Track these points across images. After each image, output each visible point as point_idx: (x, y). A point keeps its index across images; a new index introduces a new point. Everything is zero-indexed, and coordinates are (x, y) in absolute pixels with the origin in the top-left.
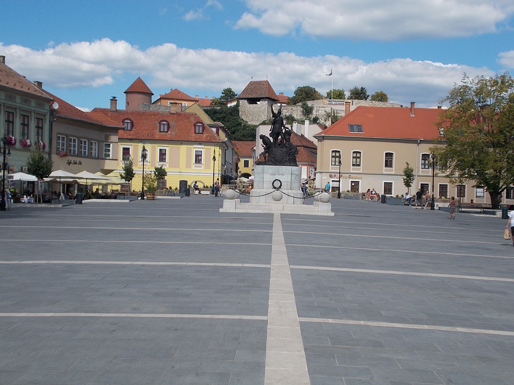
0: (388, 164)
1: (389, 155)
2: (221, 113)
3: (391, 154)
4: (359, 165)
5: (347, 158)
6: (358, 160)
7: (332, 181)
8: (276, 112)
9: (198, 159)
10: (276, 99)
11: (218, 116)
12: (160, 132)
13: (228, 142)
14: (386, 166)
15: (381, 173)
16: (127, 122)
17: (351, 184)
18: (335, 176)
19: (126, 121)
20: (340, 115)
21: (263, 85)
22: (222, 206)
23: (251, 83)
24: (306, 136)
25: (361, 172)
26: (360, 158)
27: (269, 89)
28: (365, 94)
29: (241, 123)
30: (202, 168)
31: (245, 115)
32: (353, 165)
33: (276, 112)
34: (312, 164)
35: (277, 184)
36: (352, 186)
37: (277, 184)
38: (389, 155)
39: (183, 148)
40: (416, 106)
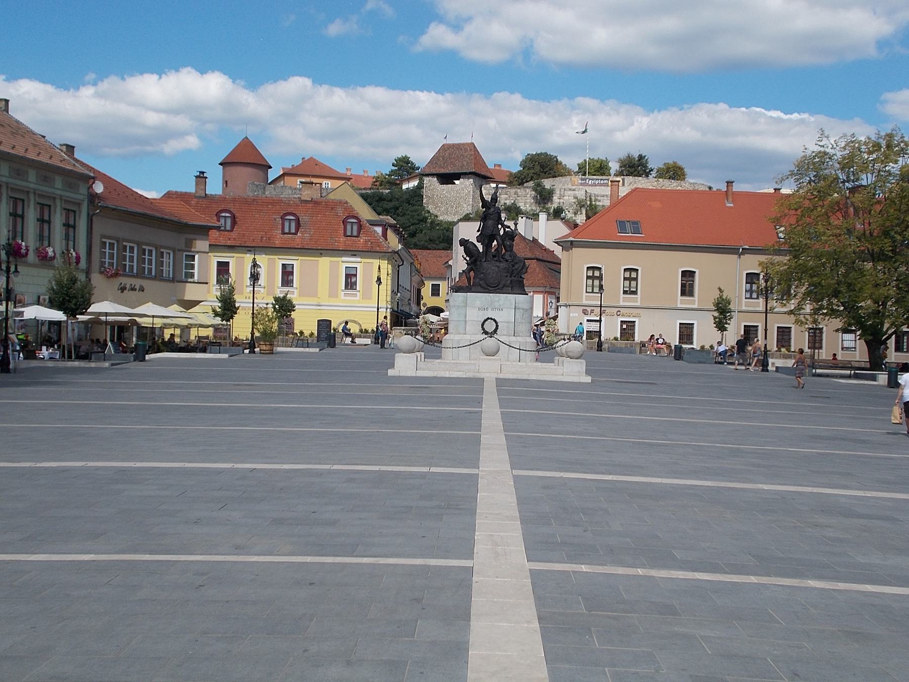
0: (687, 290)
1: (688, 275)
2: (391, 201)
3: (692, 273)
4: (635, 293)
5: (614, 280)
6: (633, 283)
7: (588, 321)
8: (488, 198)
9: (350, 282)
10: (489, 175)
11: (385, 206)
12: (284, 233)
13: (403, 252)
14: (683, 293)
15: (673, 306)
16: (225, 217)
17: (621, 326)
18: (592, 311)
19: (223, 214)
20: (601, 204)
21: (466, 150)
22: (392, 366)
23: (444, 148)
24: (542, 241)
25: (638, 304)
26: (636, 279)
27: (476, 158)
28: (645, 166)
29: (426, 218)
30: (358, 298)
31: (433, 203)
32: (625, 292)
33: (488, 198)
34: (552, 290)
35: (490, 327)
36: (622, 329)
37: (490, 327)
38: (688, 275)
39: (324, 263)
40: (736, 188)
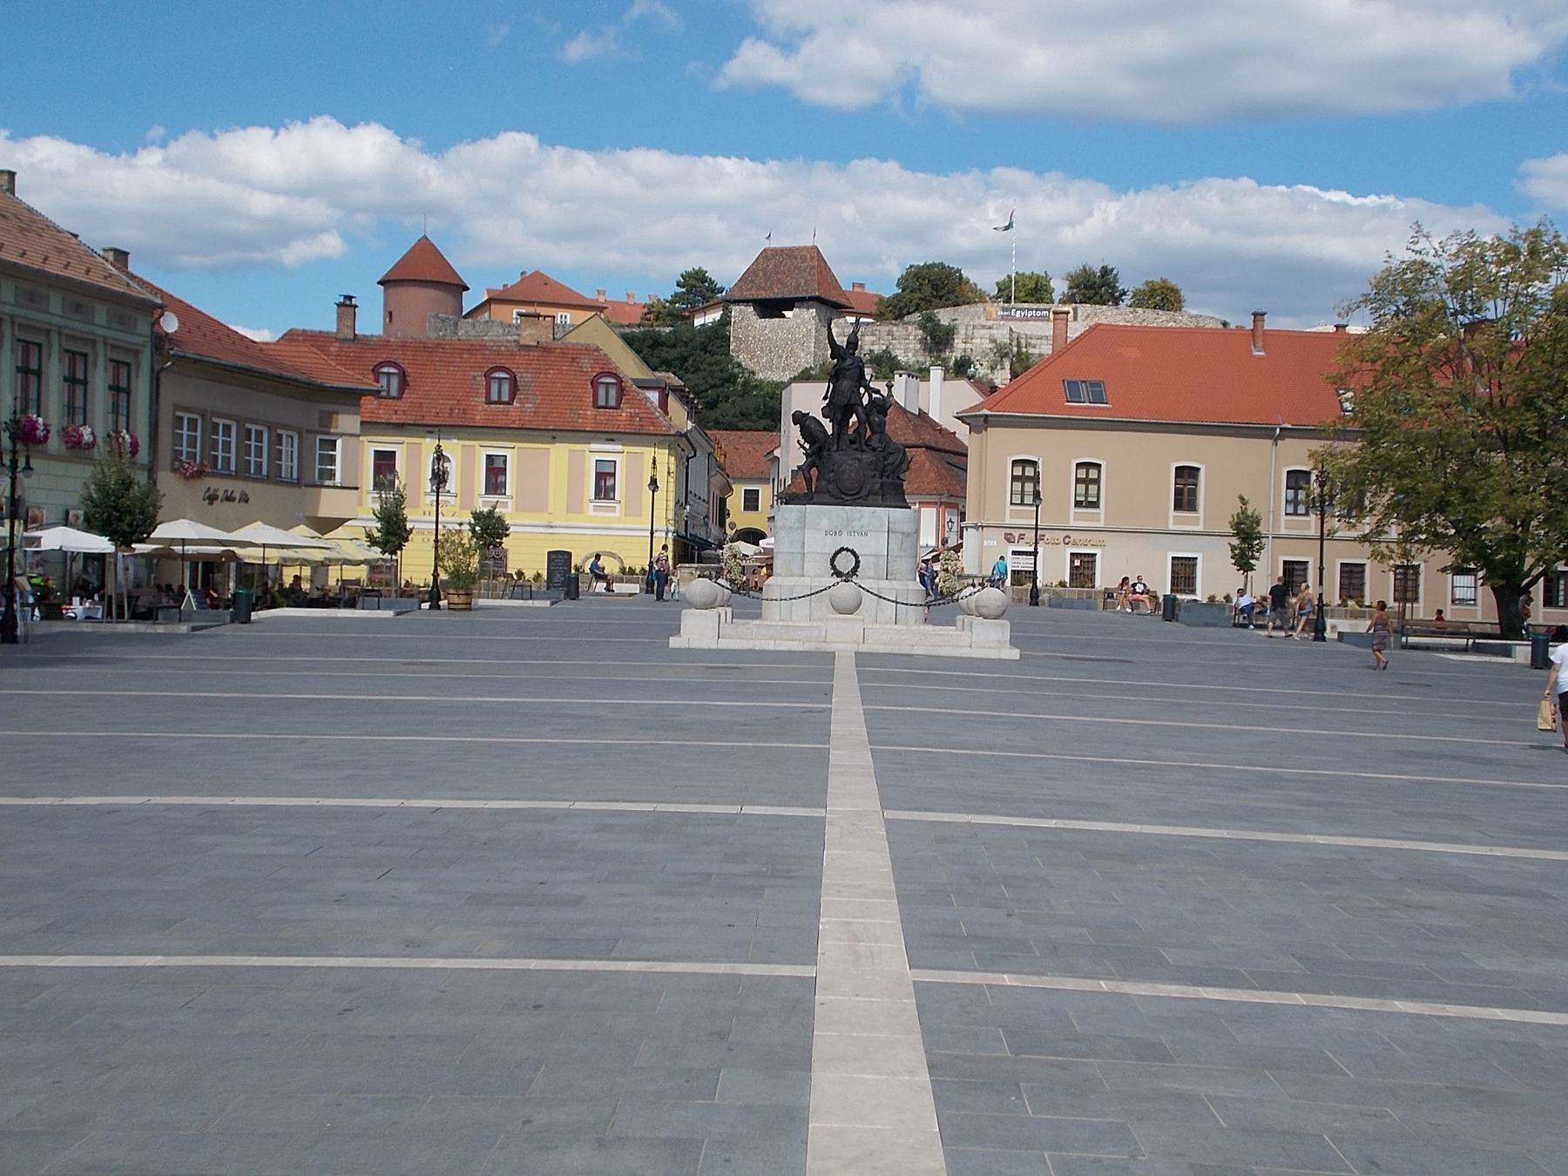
0: (1185, 500)
1: (1187, 475)
2: (674, 346)
3: (1194, 472)
4: (1095, 505)
5: (1060, 483)
6: (1093, 489)
7: (1014, 553)
8: (842, 341)
9: (604, 485)
10: (843, 301)
11: (664, 355)
12: (489, 402)
13: (695, 434)
14: (1178, 506)
15: (1161, 528)
16: (389, 374)
17: (1072, 562)
18: (1021, 537)
19: (385, 370)
20: (1036, 351)
21: (804, 259)
22: (676, 631)
23: (766, 255)
24: (934, 415)
25: (1101, 524)
26: (1097, 481)
27: (820, 273)
28: (1112, 286)
29: (736, 376)
30: (617, 514)
31: (747, 350)
32: (1078, 504)
33: (842, 341)
34: (953, 500)
35: (845, 563)
36: (1073, 568)
37: (845, 563)
38: (1187, 475)
39: (560, 453)
40: (1270, 324)
